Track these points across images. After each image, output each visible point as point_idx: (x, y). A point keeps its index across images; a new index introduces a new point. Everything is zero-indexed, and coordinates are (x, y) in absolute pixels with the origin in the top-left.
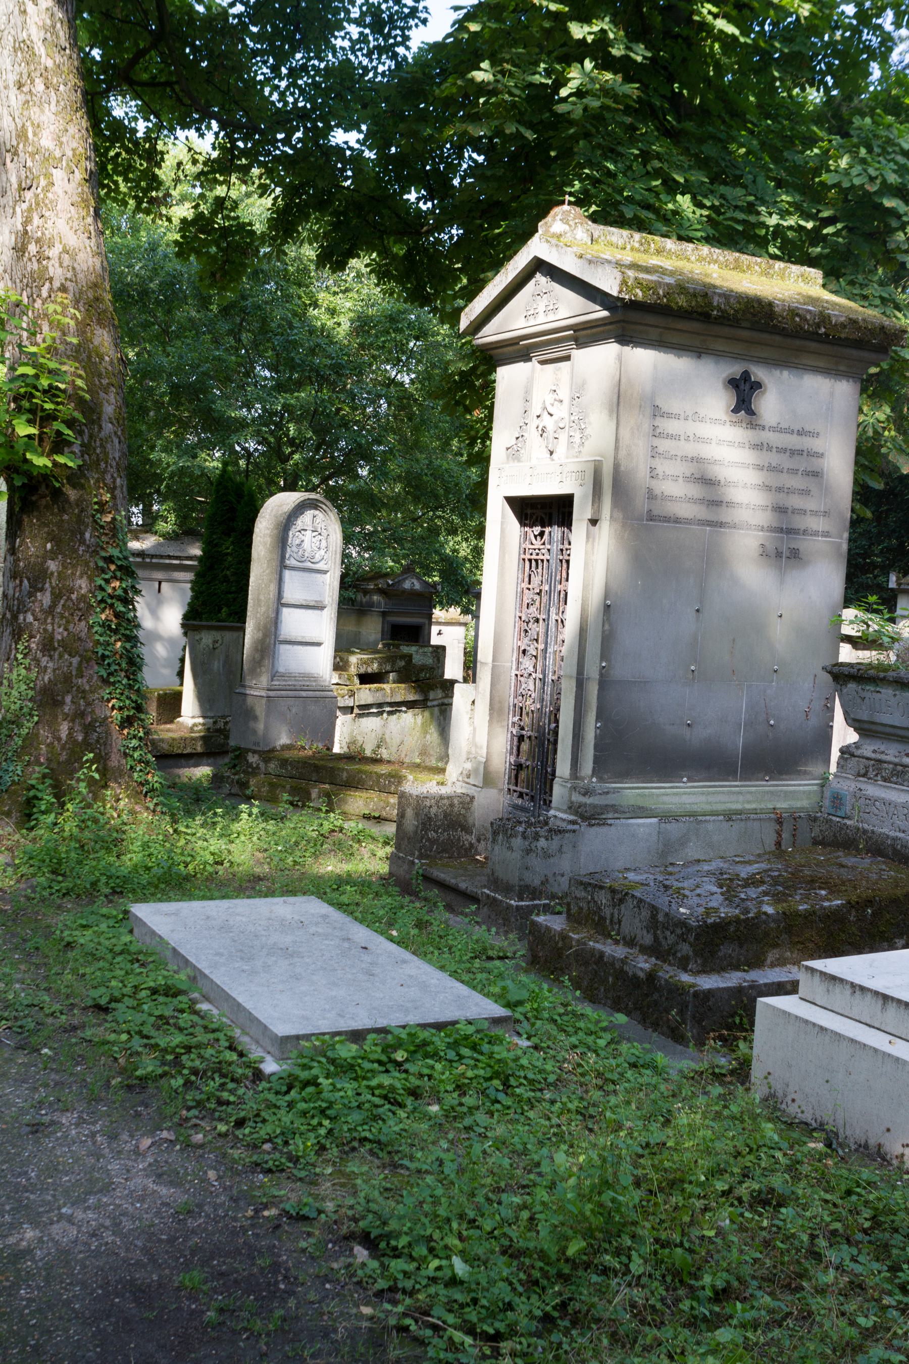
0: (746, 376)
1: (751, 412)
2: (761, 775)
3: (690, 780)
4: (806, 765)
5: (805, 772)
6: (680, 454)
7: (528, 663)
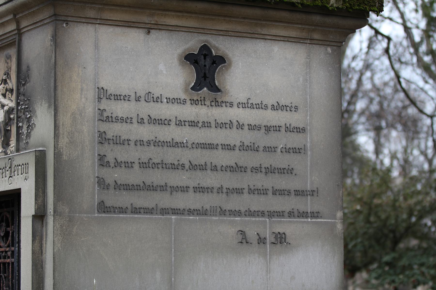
0: (205, 50)
1: (215, 89)
6: (133, 138)
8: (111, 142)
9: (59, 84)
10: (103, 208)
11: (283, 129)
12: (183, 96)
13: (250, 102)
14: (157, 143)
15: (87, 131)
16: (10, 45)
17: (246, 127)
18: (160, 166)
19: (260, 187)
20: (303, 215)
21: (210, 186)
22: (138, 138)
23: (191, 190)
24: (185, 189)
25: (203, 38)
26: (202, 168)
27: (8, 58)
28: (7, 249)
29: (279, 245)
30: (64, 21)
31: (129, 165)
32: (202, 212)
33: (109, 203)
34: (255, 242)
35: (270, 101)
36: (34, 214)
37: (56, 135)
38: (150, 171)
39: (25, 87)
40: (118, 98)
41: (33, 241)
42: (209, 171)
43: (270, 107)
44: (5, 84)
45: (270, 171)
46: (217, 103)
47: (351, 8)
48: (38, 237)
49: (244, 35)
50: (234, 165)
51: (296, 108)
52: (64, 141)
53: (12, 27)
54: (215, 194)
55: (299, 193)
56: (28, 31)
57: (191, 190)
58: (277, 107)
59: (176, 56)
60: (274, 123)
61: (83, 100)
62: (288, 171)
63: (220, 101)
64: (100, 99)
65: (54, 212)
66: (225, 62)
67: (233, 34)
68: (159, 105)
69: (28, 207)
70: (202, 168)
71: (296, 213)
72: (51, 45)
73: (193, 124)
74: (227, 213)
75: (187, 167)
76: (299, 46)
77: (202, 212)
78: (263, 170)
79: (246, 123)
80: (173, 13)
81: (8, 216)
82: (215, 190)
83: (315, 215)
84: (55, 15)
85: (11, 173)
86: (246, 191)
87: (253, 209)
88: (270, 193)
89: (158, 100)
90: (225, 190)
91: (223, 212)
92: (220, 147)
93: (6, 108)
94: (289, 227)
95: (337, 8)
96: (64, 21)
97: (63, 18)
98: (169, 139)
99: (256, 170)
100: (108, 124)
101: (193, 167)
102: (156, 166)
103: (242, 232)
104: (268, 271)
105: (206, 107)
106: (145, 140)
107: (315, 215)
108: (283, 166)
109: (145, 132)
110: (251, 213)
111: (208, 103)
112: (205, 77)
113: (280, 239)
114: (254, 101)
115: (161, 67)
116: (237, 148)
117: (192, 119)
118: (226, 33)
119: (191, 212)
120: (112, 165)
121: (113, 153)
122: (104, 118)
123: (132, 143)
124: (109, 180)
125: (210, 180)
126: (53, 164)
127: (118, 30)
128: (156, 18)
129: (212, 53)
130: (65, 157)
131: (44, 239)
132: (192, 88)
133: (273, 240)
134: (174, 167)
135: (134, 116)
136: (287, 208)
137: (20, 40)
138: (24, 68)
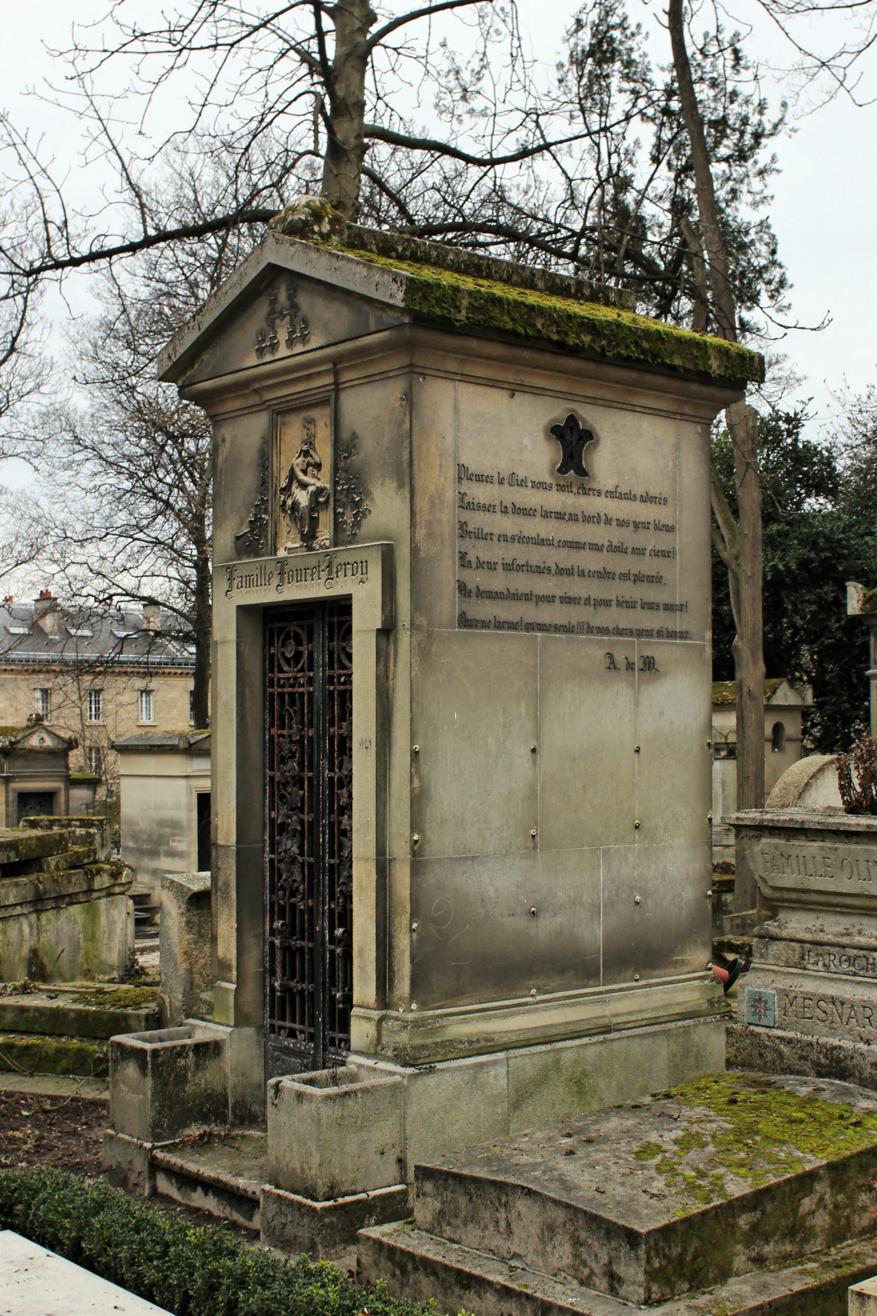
0: (572, 420)
1: (583, 472)
2: (629, 973)
3: (541, 991)
4: (682, 952)
5: (683, 963)
6: (496, 532)
7: (291, 846)
8: (473, 535)
9: (415, 457)
10: (465, 621)
11: (652, 526)
12: (549, 480)
13: (619, 490)
14: (523, 540)
15: (447, 519)
16: (324, 402)
17: (614, 523)
18: (525, 568)
19: (628, 599)
20: (672, 635)
21: (577, 596)
22: (502, 532)
23: (557, 600)
24: (550, 599)
25: (570, 405)
26: (569, 572)
27: (309, 423)
28: (300, 675)
29: (647, 672)
30: (421, 374)
31: (491, 566)
32: (567, 629)
33: (471, 615)
34: (624, 668)
35: (639, 491)
36: (380, 626)
37: (413, 525)
38: (514, 574)
39: (349, 461)
40: (480, 478)
41: (378, 662)
42: (576, 577)
43: (639, 498)
44: (305, 456)
45: (638, 578)
46: (585, 491)
47: (733, 376)
48: (383, 657)
49: (614, 404)
50: (602, 570)
51: (665, 500)
52: (421, 533)
53: (329, 380)
54: (583, 606)
55: (669, 607)
56: (352, 386)
57: (557, 600)
58: (647, 499)
59: (541, 427)
60: (642, 519)
61: (442, 479)
62: (655, 580)
63: (587, 487)
64: (460, 479)
65: (412, 624)
66: (591, 438)
67: (601, 402)
68: (522, 490)
69: (366, 618)
70: (569, 572)
71: (665, 633)
72: (402, 406)
73: (560, 516)
74: (595, 631)
75: (553, 571)
76: (668, 422)
77: (567, 629)
78: (632, 577)
79: (614, 518)
80: (542, 372)
81: (299, 631)
82: (582, 602)
83: (684, 635)
84: (411, 365)
85: (330, 572)
86: (614, 603)
87: (621, 626)
88: (639, 606)
89: (522, 483)
90: (592, 602)
91: (590, 630)
92: (587, 547)
93: (311, 489)
94: (660, 651)
95: (719, 375)
96: (421, 374)
97: (420, 370)
98: (534, 535)
99: (625, 577)
100: (469, 512)
101: (562, 572)
102: (520, 568)
103: (610, 655)
104: (637, 704)
105: (572, 495)
106: (509, 534)
107: (684, 635)
108: (652, 574)
109: (508, 525)
110: (619, 632)
111: (575, 490)
112: (571, 456)
113: (649, 664)
114: (623, 489)
115: (526, 441)
116: (605, 549)
117: (558, 509)
118: (593, 401)
119: (558, 628)
120: (474, 565)
121: (477, 551)
122: (466, 505)
123: (495, 538)
124: (471, 586)
125: (578, 588)
126: (408, 562)
127: (479, 389)
128: (522, 377)
129: (578, 424)
130: (423, 554)
131: (392, 661)
132: (559, 470)
133: (642, 666)
134: (541, 571)
135: (497, 503)
136: (655, 626)
137: (337, 399)
138: (345, 435)
